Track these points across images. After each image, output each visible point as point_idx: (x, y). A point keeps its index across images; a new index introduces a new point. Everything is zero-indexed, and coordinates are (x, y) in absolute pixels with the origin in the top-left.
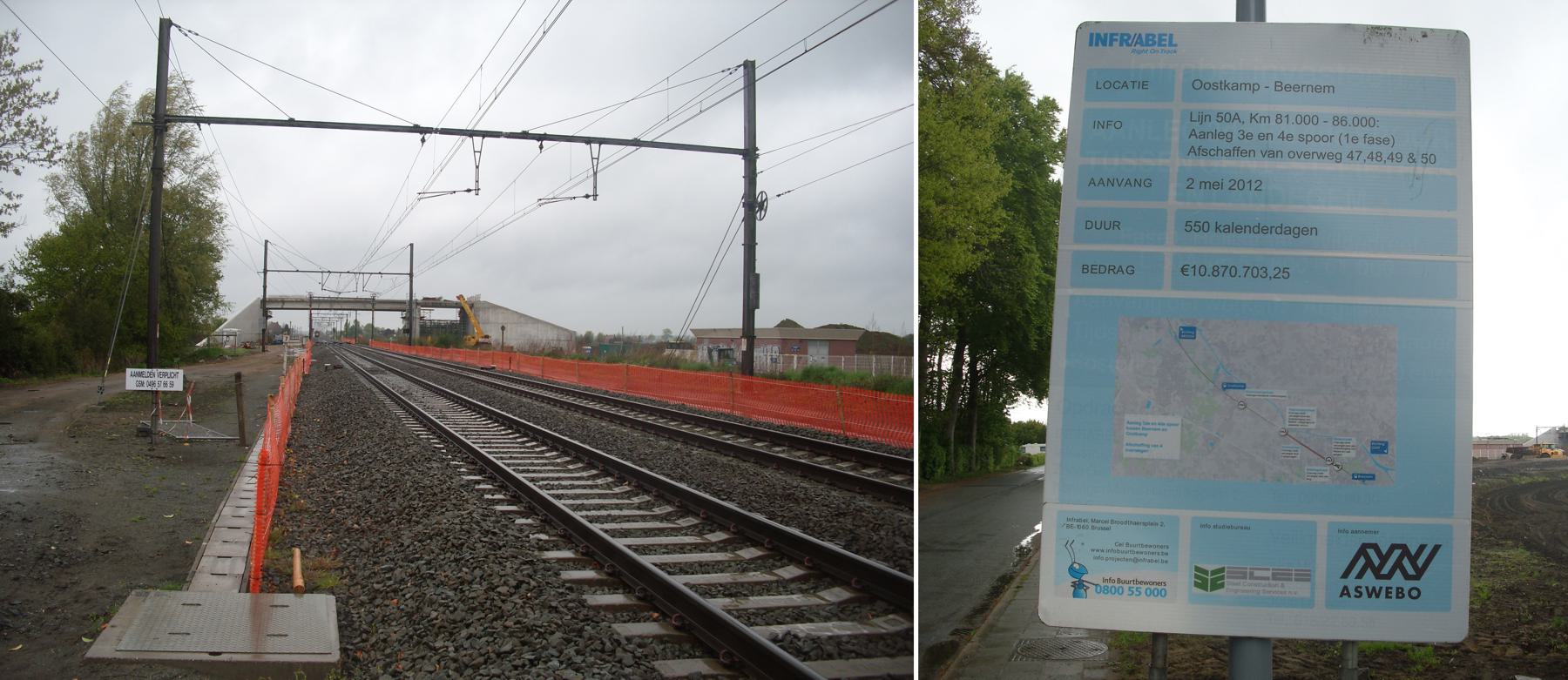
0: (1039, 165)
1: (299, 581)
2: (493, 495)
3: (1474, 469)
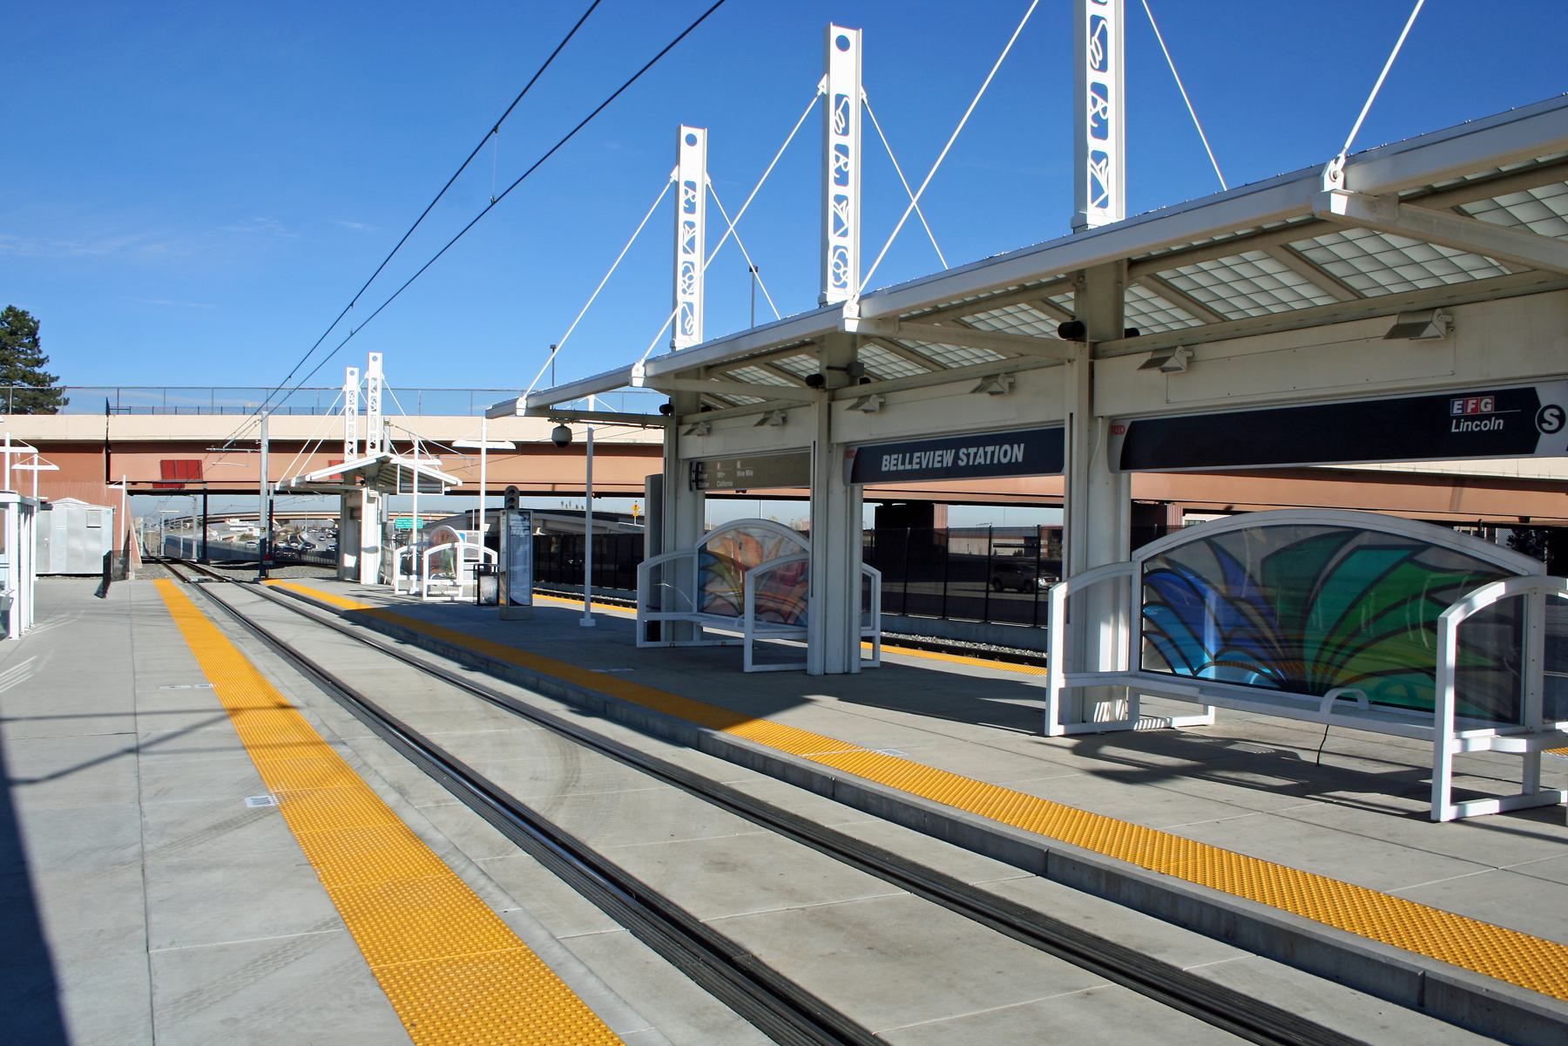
0: (989, 562)
3: (666, 611)
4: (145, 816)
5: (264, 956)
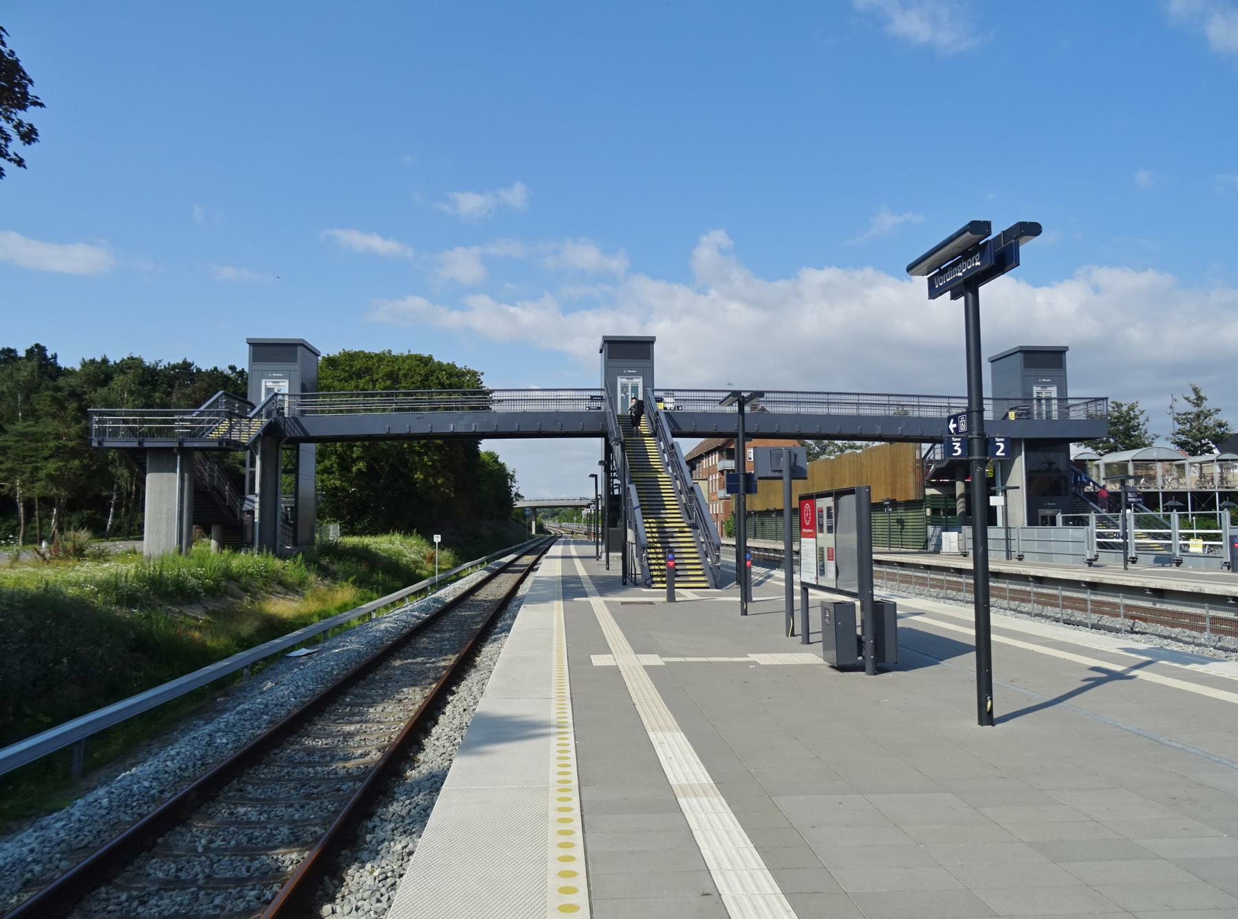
3: (1186, 493)
4: (829, 509)
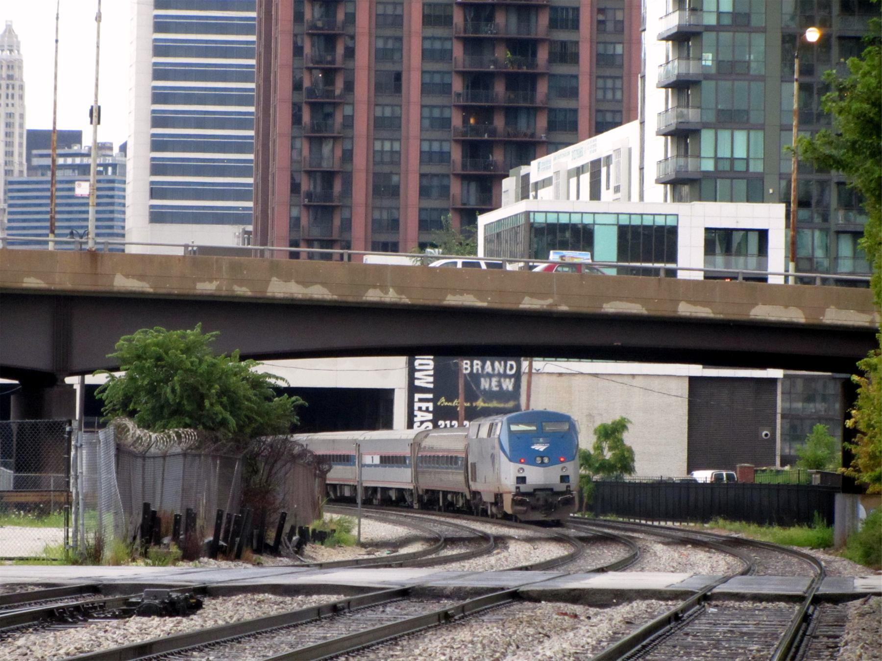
1: (441, 493)
2: (35, 422)
3: (438, 491)
5: (813, 581)
